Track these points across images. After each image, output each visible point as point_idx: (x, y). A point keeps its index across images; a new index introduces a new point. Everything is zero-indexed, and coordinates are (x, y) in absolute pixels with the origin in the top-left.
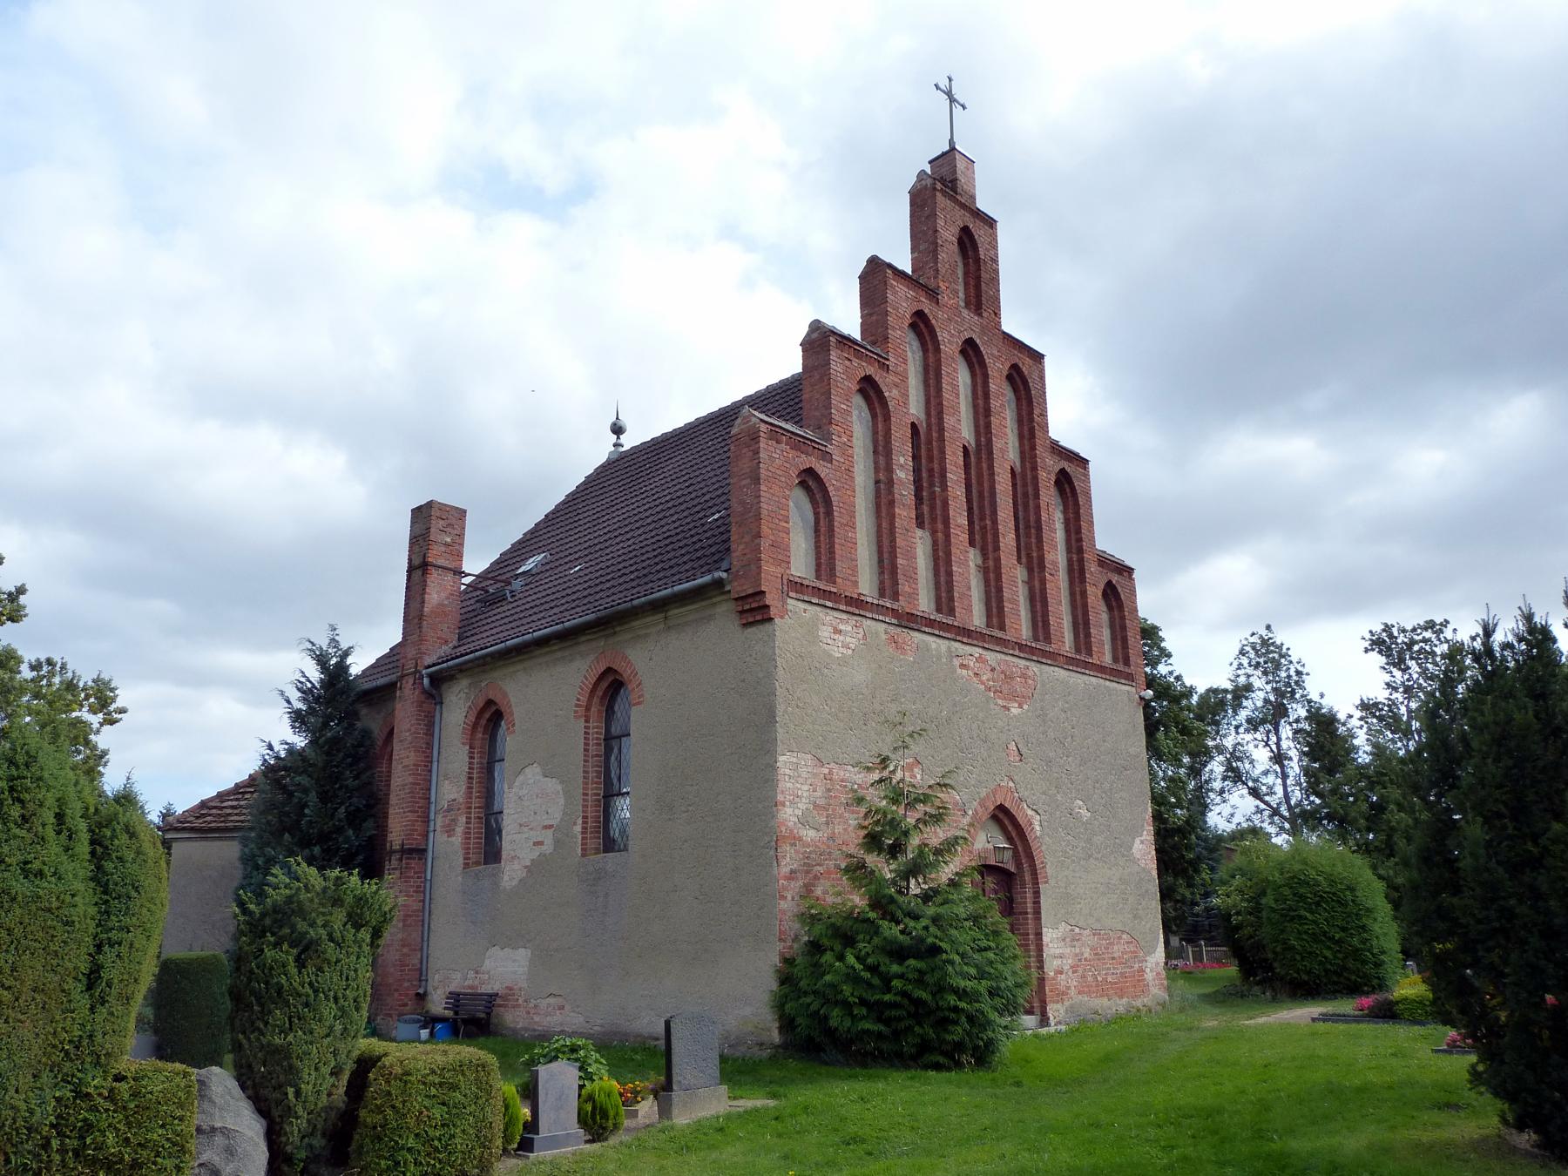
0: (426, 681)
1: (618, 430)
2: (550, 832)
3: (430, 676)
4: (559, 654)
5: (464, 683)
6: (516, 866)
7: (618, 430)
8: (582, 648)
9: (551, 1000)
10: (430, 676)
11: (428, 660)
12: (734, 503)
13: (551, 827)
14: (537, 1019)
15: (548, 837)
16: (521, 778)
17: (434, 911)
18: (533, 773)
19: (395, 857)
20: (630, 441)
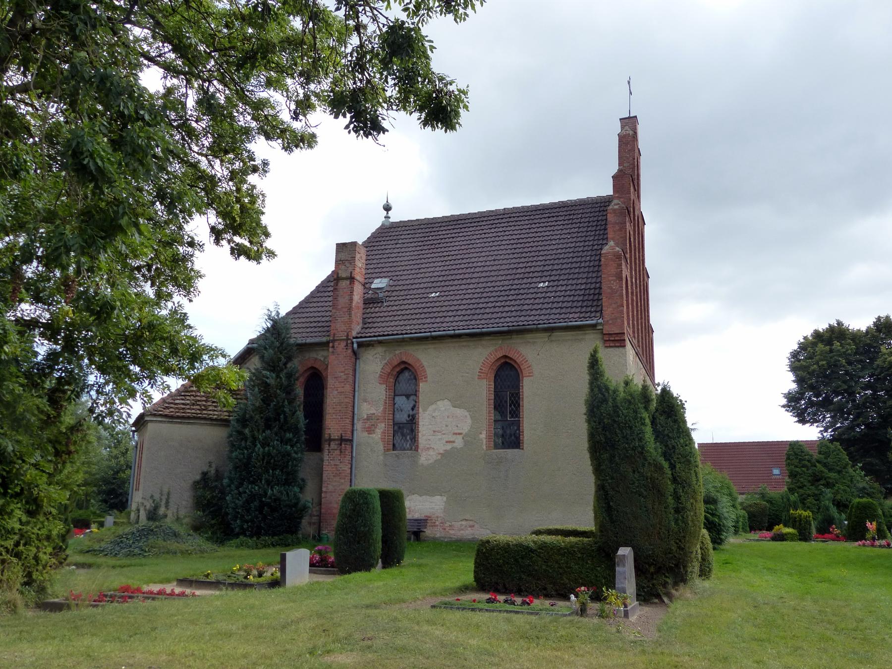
0: (355, 345)
1: (387, 208)
2: (460, 437)
3: (358, 343)
4: (464, 344)
5: (380, 350)
6: (431, 452)
7: (387, 208)
8: (484, 342)
9: (463, 523)
10: (358, 343)
11: (354, 334)
12: (604, 287)
13: (460, 434)
14: (452, 532)
15: (459, 442)
16: (434, 406)
17: (190, 426)
18: (257, 357)
19: (333, 445)
20: (396, 216)
